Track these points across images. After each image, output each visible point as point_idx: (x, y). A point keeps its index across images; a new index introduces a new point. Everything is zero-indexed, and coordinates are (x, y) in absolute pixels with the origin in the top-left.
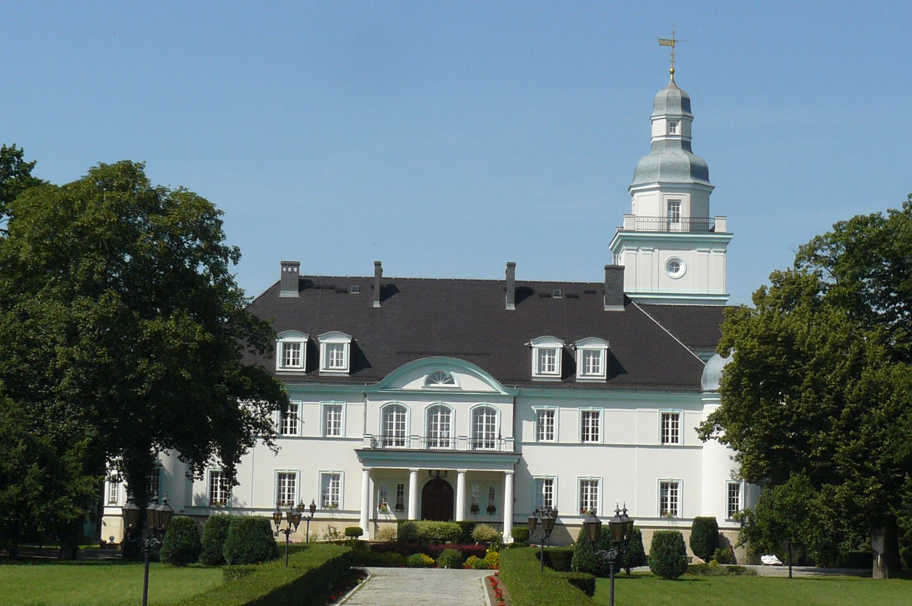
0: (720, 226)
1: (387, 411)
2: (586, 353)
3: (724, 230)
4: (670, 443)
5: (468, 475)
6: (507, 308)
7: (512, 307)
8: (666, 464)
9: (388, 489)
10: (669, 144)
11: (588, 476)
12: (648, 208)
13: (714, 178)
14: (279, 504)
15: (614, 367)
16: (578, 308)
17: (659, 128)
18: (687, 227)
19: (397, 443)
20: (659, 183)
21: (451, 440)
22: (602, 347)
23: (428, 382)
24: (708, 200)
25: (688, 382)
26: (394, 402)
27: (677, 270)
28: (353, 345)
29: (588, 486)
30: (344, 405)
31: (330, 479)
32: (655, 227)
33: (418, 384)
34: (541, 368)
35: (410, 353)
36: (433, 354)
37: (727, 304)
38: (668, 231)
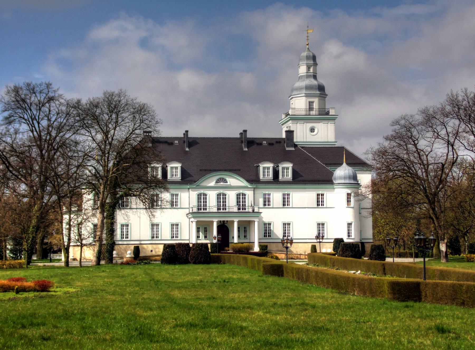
0: (332, 112)
1: (199, 196)
2: (283, 168)
3: (334, 114)
4: (320, 206)
5: (239, 222)
6: (244, 150)
7: (246, 149)
8: (320, 215)
9: (203, 228)
10: (308, 77)
11: (286, 221)
12: (299, 104)
13: (327, 91)
14: (284, 236)
15: (295, 173)
16: (281, 148)
17: (303, 70)
18: (317, 113)
19: (223, 209)
20: (305, 94)
21: (227, 208)
22: (179, 165)
23: (217, 182)
24: (325, 100)
25: (327, 181)
26: (202, 191)
27: (314, 132)
28: (182, 167)
29: (286, 225)
30: (179, 194)
31: (175, 226)
32: (304, 113)
33: (213, 184)
34: (264, 175)
35: (205, 170)
36: (220, 170)
37: (336, 146)
38: (309, 115)
